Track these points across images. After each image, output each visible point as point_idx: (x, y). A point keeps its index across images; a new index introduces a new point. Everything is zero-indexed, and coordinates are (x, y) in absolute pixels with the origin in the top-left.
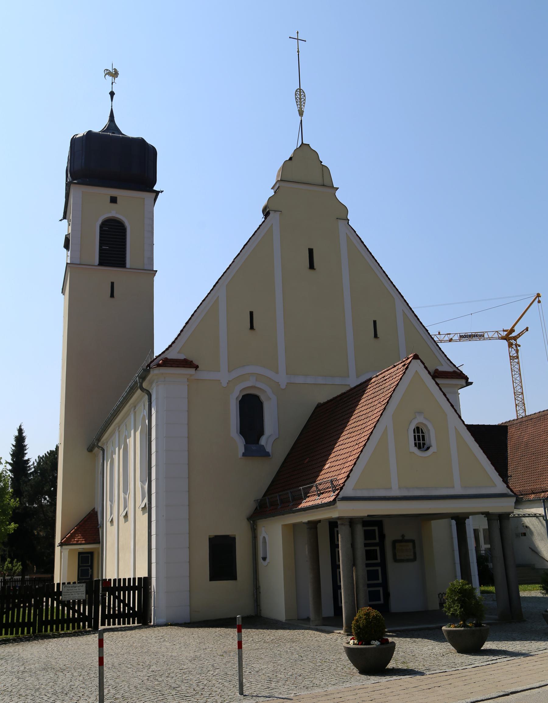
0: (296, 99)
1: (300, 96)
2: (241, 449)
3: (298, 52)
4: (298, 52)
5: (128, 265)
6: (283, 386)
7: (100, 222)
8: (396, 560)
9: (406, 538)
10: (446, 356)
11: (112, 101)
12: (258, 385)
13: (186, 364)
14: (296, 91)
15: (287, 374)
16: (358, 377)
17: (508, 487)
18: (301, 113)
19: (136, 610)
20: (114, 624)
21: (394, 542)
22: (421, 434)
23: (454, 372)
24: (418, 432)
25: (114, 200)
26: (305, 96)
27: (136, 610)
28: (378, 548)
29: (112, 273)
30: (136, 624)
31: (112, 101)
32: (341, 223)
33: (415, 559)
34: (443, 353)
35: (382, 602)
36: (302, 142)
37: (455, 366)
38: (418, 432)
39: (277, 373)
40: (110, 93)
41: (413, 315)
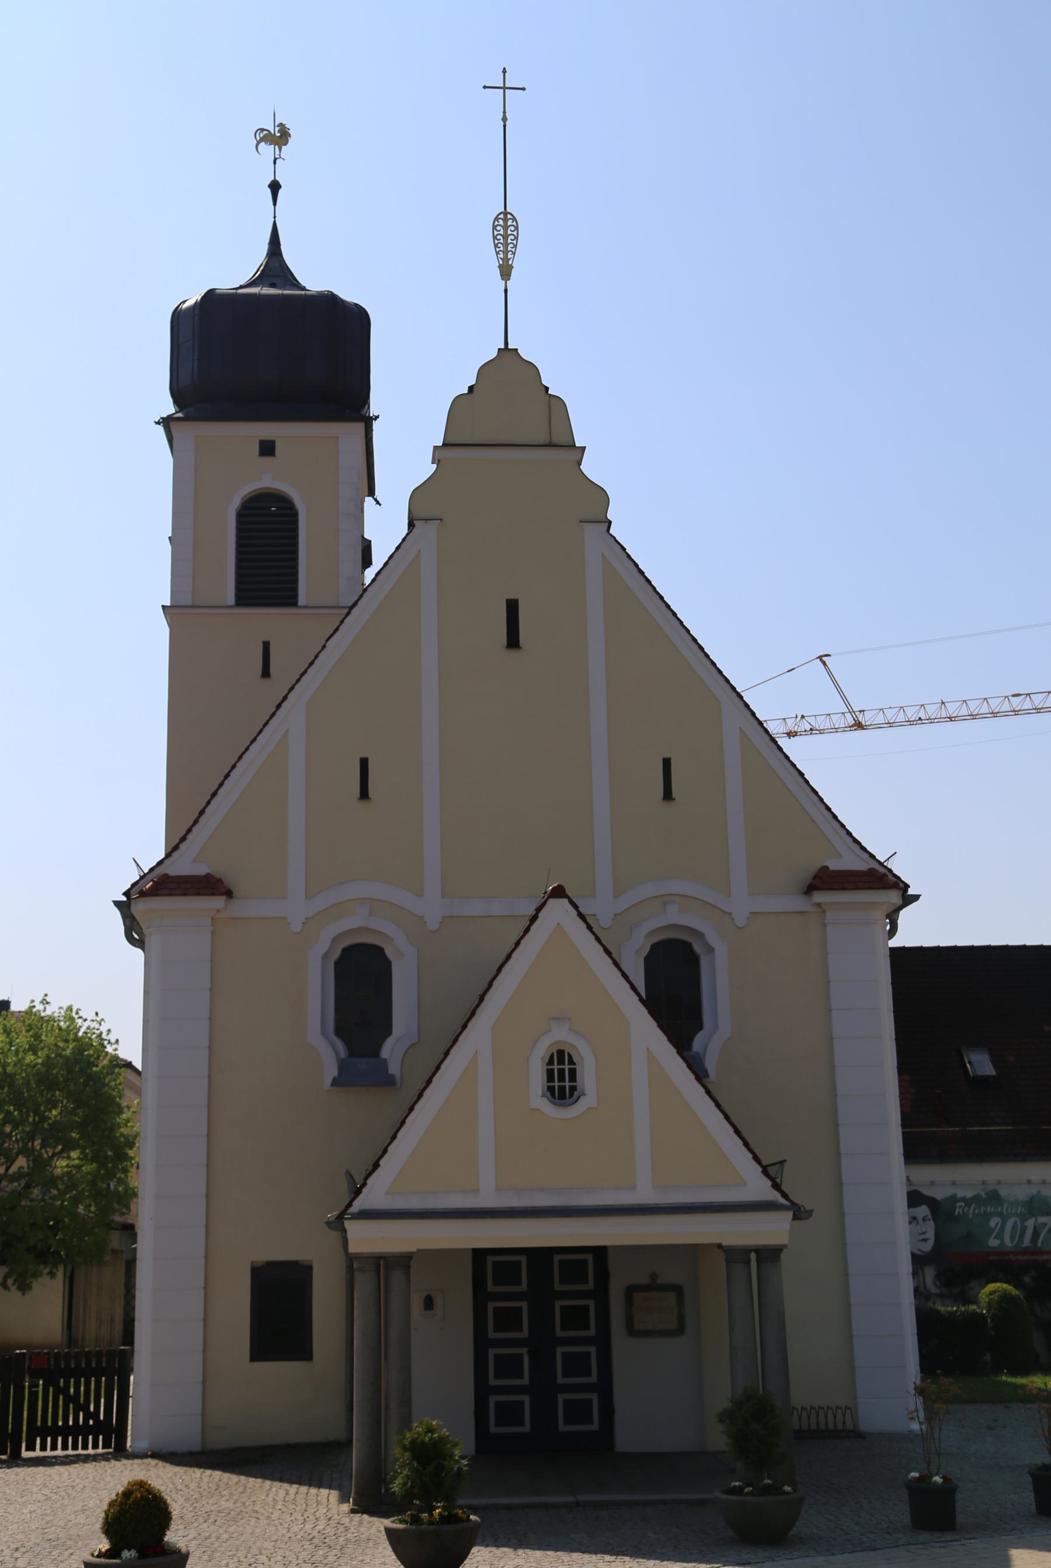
0: (495, 238)
1: (505, 229)
2: (331, 1071)
3: (504, 119)
4: (504, 119)
5: (302, 600)
6: (433, 925)
7: (236, 504)
8: (632, 1331)
9: (661, 1281)
10: (849, 833)
11: (275, 204)
12: (377, 924)
13: (209, 885)
14: (497, 219)
15: (443, 897)
16: (617, 893)
17: (776, 1186)
18: (506, 272)
19: (102, 1418)
20: (43, 1448)
21: (631, 1291)
22: (567, 1067)
23: (871, 872)
24: (561, 1062)
25: (267, 449)
26: (517, 228)
27: (102, 1418)
28: (591, 1304)
29: (266, 622)
30: (100, 1450)
31: (275, 204)
32: (592, 531)
33: (680, 1330)
34: (843, 826)
35: (595, 1426)
36: (506, 343)
37: (872, 856)
38: (561, 1062)
39: (420, 894)
40: (270, 186)
41: (767, 738)
